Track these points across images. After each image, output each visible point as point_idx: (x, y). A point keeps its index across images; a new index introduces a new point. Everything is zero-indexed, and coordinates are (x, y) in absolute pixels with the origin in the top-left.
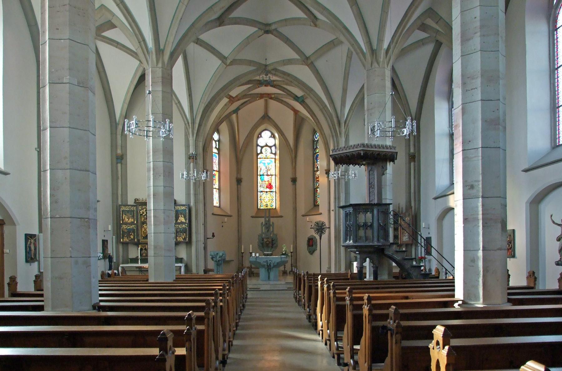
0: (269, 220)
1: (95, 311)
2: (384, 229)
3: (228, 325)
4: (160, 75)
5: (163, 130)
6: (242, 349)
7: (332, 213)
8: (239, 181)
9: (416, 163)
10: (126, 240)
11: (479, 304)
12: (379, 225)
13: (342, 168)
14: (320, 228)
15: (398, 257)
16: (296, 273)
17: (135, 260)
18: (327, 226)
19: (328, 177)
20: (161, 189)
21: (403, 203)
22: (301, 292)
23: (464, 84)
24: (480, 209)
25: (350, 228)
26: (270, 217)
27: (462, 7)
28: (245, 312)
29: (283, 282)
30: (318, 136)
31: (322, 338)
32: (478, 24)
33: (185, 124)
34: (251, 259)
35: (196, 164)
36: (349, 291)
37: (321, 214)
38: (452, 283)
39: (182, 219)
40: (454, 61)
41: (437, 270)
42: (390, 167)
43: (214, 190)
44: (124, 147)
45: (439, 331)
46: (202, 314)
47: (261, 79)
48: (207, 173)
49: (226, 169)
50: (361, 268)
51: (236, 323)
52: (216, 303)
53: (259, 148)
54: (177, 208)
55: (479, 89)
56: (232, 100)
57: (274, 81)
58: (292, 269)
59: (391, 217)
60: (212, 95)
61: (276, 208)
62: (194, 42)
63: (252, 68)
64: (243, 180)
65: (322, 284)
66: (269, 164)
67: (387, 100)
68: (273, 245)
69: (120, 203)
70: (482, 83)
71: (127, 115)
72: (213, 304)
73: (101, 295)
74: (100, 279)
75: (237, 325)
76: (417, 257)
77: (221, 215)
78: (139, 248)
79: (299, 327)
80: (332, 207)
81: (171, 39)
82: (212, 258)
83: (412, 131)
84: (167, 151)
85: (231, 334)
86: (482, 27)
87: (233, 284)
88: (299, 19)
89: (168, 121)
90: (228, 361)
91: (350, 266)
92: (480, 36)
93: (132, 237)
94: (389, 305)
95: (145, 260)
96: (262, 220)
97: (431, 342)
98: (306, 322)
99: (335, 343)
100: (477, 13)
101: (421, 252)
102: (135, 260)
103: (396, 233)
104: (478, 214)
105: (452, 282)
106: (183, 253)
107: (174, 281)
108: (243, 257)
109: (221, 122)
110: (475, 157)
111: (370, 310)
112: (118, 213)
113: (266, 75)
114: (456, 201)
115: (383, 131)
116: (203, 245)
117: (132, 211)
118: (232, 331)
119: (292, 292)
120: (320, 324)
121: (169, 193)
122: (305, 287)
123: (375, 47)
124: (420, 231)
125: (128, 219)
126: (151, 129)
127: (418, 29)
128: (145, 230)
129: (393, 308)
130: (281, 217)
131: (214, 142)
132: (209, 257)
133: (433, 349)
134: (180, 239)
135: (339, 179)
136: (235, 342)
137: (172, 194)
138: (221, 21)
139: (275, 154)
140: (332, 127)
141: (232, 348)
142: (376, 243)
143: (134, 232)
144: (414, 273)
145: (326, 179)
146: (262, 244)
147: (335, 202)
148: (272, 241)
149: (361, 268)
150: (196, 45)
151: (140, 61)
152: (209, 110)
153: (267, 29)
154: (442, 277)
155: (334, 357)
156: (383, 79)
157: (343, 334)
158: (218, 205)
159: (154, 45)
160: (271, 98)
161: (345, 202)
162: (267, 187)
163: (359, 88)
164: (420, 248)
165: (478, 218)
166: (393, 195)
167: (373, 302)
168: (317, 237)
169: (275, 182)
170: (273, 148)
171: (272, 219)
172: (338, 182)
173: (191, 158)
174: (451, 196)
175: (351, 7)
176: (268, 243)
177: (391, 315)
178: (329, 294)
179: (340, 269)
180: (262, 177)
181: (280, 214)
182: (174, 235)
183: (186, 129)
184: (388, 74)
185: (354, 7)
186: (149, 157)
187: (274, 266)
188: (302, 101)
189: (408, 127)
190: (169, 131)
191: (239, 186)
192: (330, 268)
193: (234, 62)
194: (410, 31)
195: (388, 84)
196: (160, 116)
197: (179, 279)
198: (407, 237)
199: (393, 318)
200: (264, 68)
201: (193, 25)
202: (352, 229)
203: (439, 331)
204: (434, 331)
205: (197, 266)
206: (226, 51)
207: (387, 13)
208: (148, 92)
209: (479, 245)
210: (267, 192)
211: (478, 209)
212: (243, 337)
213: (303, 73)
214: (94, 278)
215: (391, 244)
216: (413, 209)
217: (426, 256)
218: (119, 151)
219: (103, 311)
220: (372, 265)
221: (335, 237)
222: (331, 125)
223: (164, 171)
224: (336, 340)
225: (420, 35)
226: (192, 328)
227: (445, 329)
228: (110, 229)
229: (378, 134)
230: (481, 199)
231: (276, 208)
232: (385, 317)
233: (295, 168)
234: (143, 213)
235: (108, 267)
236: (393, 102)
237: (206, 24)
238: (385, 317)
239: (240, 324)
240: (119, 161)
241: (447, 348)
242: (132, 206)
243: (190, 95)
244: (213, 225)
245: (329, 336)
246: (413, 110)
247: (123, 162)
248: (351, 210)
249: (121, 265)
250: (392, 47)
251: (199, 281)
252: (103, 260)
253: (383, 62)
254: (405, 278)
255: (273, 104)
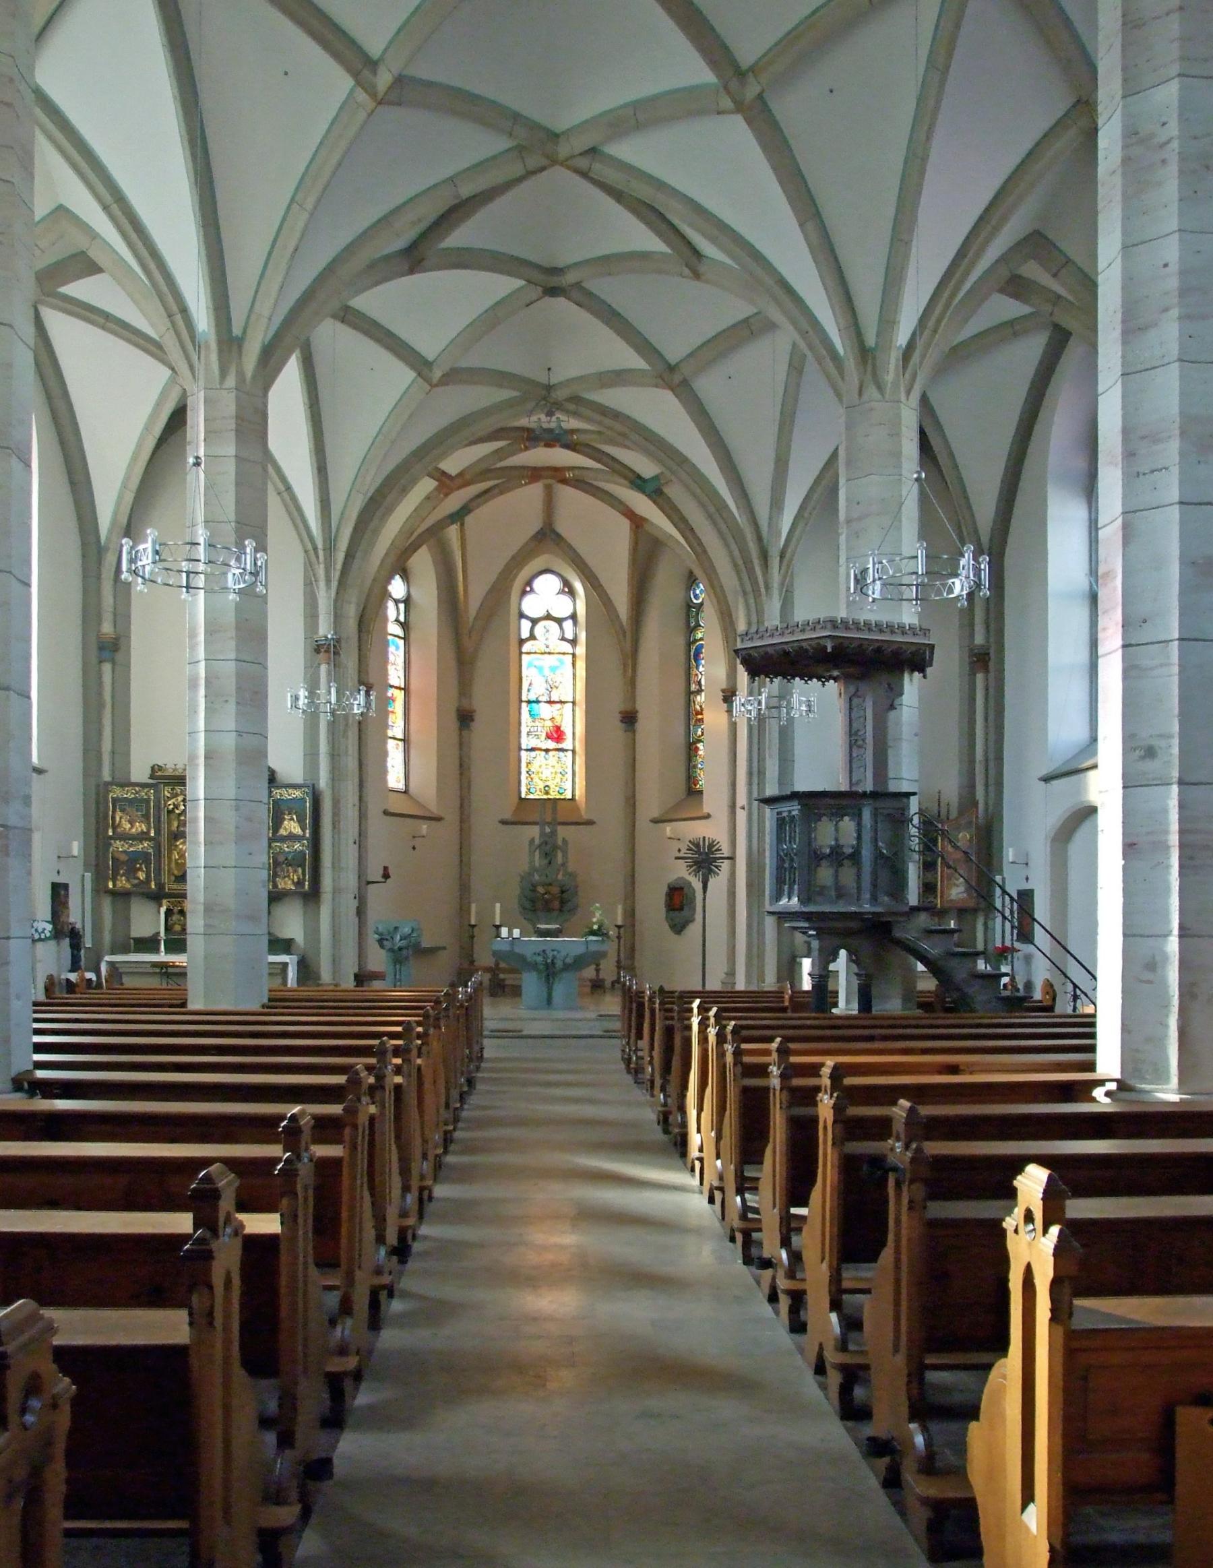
0: (554, 833)
1: (19, 1095)
2: (891, 868)
3: (418, 1142)
4: (232, 409)
5: (237, 572)
6: (461, 1212)
7: (741, 816)
8: (465, 718)
9: (992, 675)
10: (123, 883)
11: (1169, 1094)
12: (878, 856)
13: (773, 686)
14: (704, 859)
15: (933, 948)
16: (630, 987)
17: (149, 944)
18: (726, 852)
19: (730, 711)
20: (229, 742)
21: (950, 788)
22: (644, 1044)
23: (1129, 455)
24: (1174, 816)
25: (792, 860)
26: (555, 823)
27: (1125, 233)
28: (473, 1100)
29: (593, 1015)
30: (700, 593)
31: (701, 1183)
32: (1173, 283)
33: (306, 552)
34: (498, 945)
35: (336, 665)
36: (778, 1050)
37: (708, 816)
38: (1087, 1027)
39: (291, 826)
40: (1100, 389)
41: (1049, 987)
42: (912, 686)
43: (391, 744)
44: (122, 617)
45: (1033, 1182)
46: (336, 1109)
47: (533, 425)
48: (367, 694)
49: (427, 681)
50: (822, 979)
51: (446, 1133)
52: (380, 1078)
53: (525, 626)
54: (277, 793)
55: (1175, 470)
56: (446, 483)
57: (573, 431)
58: (619, 977)
59: (914, 831)
60: (390, 466)
61: (573, 799)
62: (334, 316)
63: (506, 394)
64: (477, 717)
65: (703, 1025)
66: (553, 669)
67: (904, 493)
68: (563, 903)
69: (107, 777)
70: (1182, 454)
71: (131, 529)
72: (372, 1080)
73: (39, 1048)
74: (42, 997)
75: (447, 1140)
76: (990, 947)
77: (408, 814)
78: (163, 910)
79: (636, 1148)
80: (742, 799)
81: (264, 307)
82: (381, 942)
83: (978, 585)
84: (249, 631)
85: (426, 1166)
86: (1184, 292)
87: (437, 1019)
88: (644, 256)
89: (249, 545)
90: (417, 1247)
91: (790, 969)
92: (1180, 318)
93: (142, 876)
94: (890, 1095)
95: (177, 944)
96: (534, 832)
97: (1010, 1212)
98: (658, 1135)
99: (738, 1199)
100: (1171, 251)
101: (1002, 932)
102: (149, 944)
103: (929, 875)
104: (1167, 832)
105: (1089, 1022)
106: (292, 924)
107: (263, 1006)
108: (472, 937)
109: (413, 548)
110: (1161, 665)
111: (838, 1109)
112: (99, 808)
113: (550, 414)
114: (1104, 787)
115: (892, 585)
116: (355, 903)
117: (142, 800)
118: (431, 1158)
119: (618, 1043)
120: (695, 1140)
121: (252, 753)
122: (654, 1028)
123: (871, 340)
124: (1001, 872)
125: (132, 823)
126: (201, 567)
127: (1002, 291)
128: (182, 856)
129: (902, 1108)
130: (590, 823)
131: (391, 605)
132: (372, 938)
133: (1016, 1231)
134: (286, 884)
135: (761, 718)
136: (440, 1191)
137: (264, 755)
138: (414, 257)
139: (574, 642)
140: (743, 567)
141: (430, 1208)
142: (867, 907)
143: (147, 860)
144: (979, 995)
145: (724, 717)
146: (533, 901)
147: (750, 784)
148: (563, 892)
149: (822, 979)
150: (339, 325)
151: (173, 369)
152: (378, 514)
153: (550, 282)
154: (1064, 1006)
155: (732, 1239)
156: (895, 435)
157: (761, 1170)
158: (401, 786)
159: (213, 324)
160: (564, 481)
161: (781, 783)
162: (549, 737)
163: (826, 457)
164: (999, 919)
165: (1166, 841)
166: (919, 765)
167: (849, 1081)
168: (697, 885)
169: (573, 722)
170: (568, 625)
171: (562, 832)
172: (758, 726)
173: (324, 650)
174: (1091, 774)
175: (801, 225)
176: (549, 900)
177: (899, 1126)
178: (721, 1054)
179: (762, 979)
180: (534, 705)
181: (585, 816)
182: (264, 874)
183: (309, 566)
184: (909, 418)
185: (810, 226)
186: (193, 647)
187: (567, 967)
188: (654, 490)
189: (964, 573)
190: (255, 574)
191: (465, 733)
192: (731, 973)
193: (453, 376)
194: (977, 296)
195: (910, 448)
196: (229, 529)
197: (277, 1001)
198: (962, 889)
199: (902, 1136)
200: (544, 395)
201: (330, 269)
202: (796, 864)
203: (1033, 1182)
204: (1020, 1182)
205: (335, 962)
206: (429, 345)
207: (908, 244)
208: (191, 460)
209: (1168, 921)
210: (547, 751)
211: (1167, 819)
212: (465, 1175)
213: (661, 412)
214: (18, 998)
215: (915, 909)
216: (981, 806)
217: (1017, 945)
218: (107, 628)
219: (44, 1097)
220: (855, 968)
221: (750, 886)
222: (740, 562)
223: (239, 689)
224: (740, 1191)
225: (1007, 308)
226: (299, 1158)
227: (1050, 1177)
228: (75, 852)
229: (875, 591)
230: (1175, 789)
231: (573, 799)
232: (882, 1128)
233: (632, 684)
234: (176, 807)
235: (68, 962)
236: (923, 499)
237: (372, 266)
238: (882, 1128)
239: (458, 1135)
240: (106, 654)
241: (1055, 1230)
242: (144, 786)
243: (321, 470)
244: (385, 844)
245: (721, 1178)
246: (985, 523)
247: (119, 657)
248: (795, 808)
249: (107, 958)
250: (920, 344)
251: (336, 1010)
252: (53, 943)
253: (896, 384)
254: (948, 1010)
255: (568, 496)
